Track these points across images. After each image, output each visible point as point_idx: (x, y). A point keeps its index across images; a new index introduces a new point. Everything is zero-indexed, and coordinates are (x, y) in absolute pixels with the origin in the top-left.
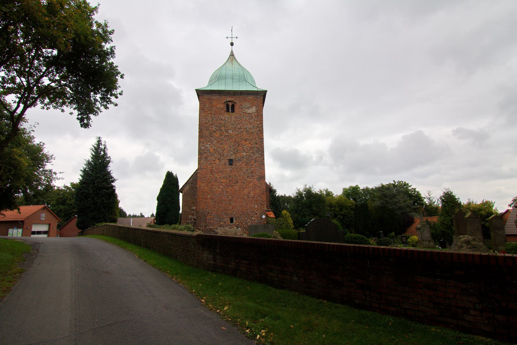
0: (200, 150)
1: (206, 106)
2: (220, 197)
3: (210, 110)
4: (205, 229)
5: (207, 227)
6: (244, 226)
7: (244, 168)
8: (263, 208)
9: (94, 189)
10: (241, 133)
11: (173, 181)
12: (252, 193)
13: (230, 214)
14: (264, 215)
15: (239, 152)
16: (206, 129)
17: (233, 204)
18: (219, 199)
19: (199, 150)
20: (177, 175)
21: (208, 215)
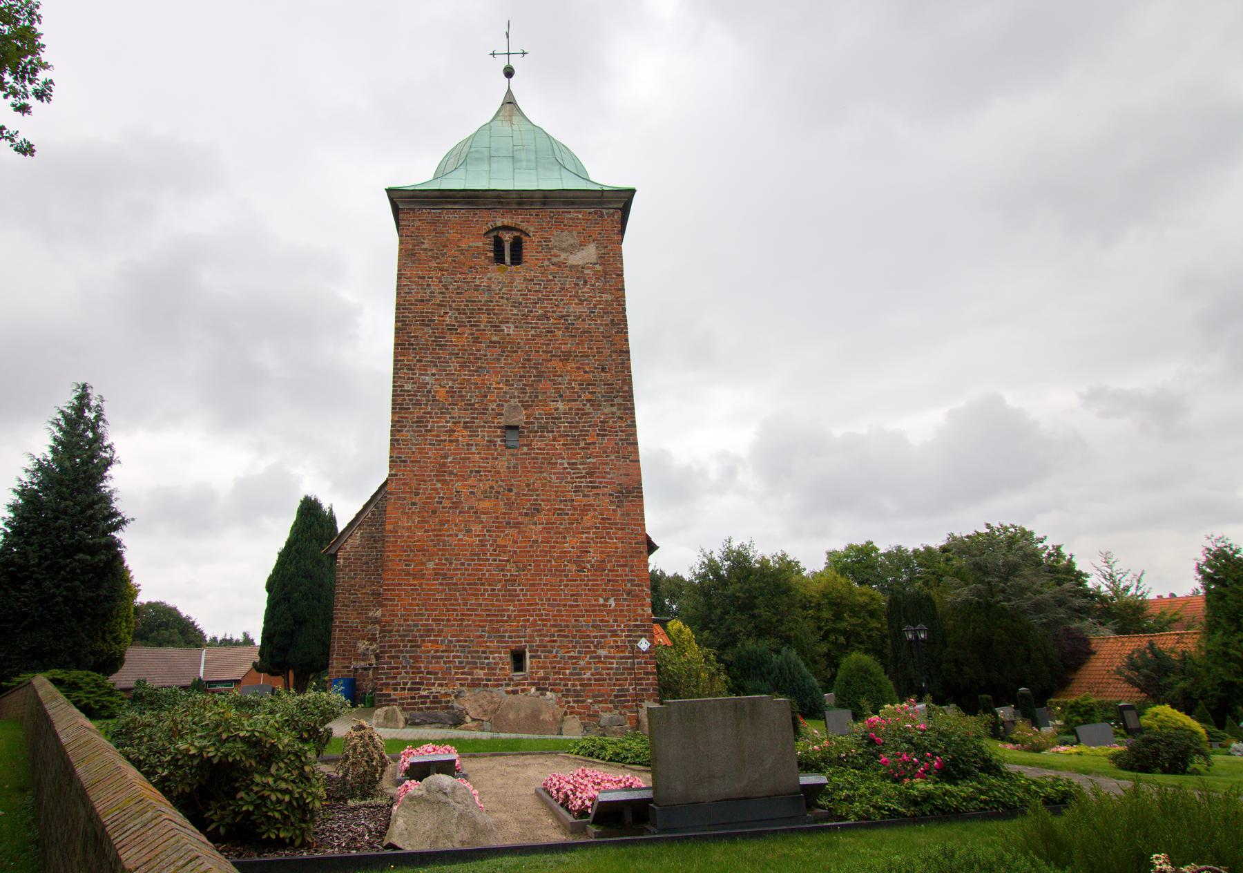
0: (398, 395)
1: (423, 243)
2: (473, 569)
3: (438, 258)
4: (414, 698)
5: (419, 689)
6: (566, 685)
7: (563, 458)
8: (640, 611)
9: (47, 550)
10: (549, 332)
11: (322, 527)
12: (595, 552)
13: (510, 637)
14: (645, 636)
15: (541, 401)
16: (423, 321)
17: (524, 595)
18: (468, 575)
19: (393, 395)
20: (334, 510)
21: (424, 641)
